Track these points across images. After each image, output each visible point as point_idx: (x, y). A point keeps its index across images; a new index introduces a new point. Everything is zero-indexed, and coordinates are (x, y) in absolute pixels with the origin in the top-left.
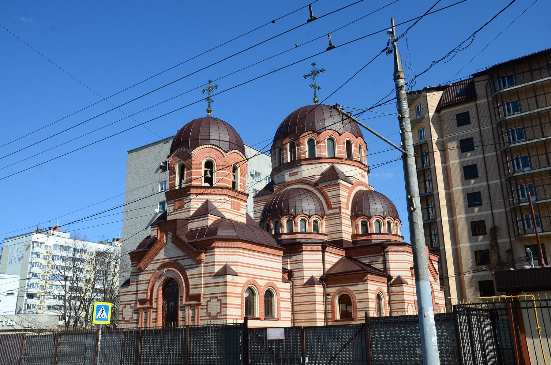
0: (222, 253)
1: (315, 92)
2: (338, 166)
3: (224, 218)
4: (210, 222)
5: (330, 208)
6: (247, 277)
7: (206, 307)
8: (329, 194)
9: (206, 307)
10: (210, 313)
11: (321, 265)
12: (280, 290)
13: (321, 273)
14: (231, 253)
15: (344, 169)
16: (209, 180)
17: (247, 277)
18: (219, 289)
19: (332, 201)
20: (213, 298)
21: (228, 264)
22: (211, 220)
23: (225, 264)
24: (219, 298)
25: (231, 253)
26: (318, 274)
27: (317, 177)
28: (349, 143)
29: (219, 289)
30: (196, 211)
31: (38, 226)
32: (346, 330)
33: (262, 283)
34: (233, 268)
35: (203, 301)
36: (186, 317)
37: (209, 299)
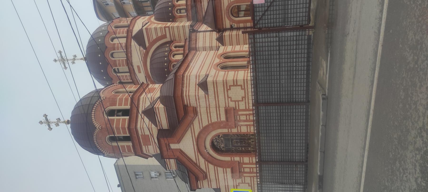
0: (188, 89)
1: (78, 59)
2: (134, 34)
3: (159, 97)
4: (161, 106)
5: (164, 36)
6: (211, 68)
7: (237, 102)
8: (155, 37)
9: (237, 102)
10: (243, 98)
11: (208, 33)
12: (225, 51)
13: (214, 33)
14: (188, 81)
15: (136, 28)
16: (125, 112)
17: (211, 68)
18: (220, 89)
19: (160, 34)
20: (228, 96)
21: (197, 83)
22: (160, 107)
23: (197, 86)
24: (228, 88)
25: (188, 81)
26: (215, 35)
27: (142, 49)
28: (117, 27)
29: (220, 89)
30: (152, 122)
31: (41, 122)
32: (276, 166)
33: (217, 61)
34: (201, 79)
35: (232, 105)
36: (246, 127)
37: (229, 99)
